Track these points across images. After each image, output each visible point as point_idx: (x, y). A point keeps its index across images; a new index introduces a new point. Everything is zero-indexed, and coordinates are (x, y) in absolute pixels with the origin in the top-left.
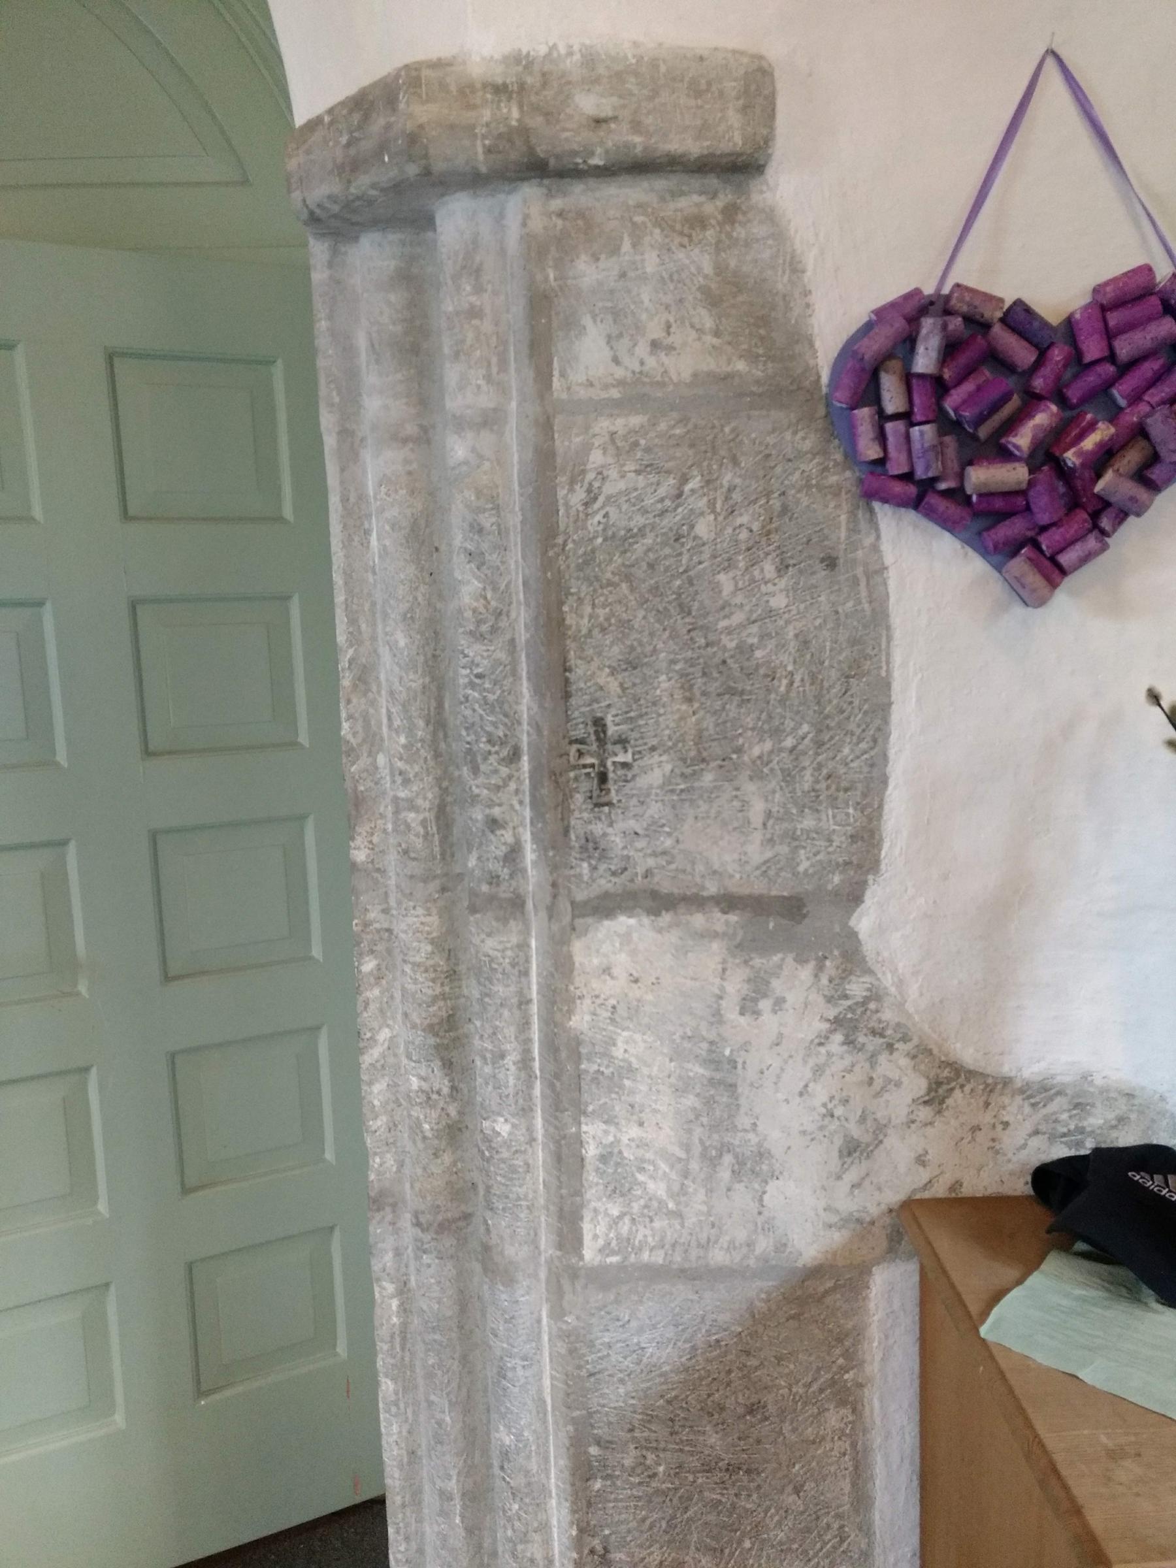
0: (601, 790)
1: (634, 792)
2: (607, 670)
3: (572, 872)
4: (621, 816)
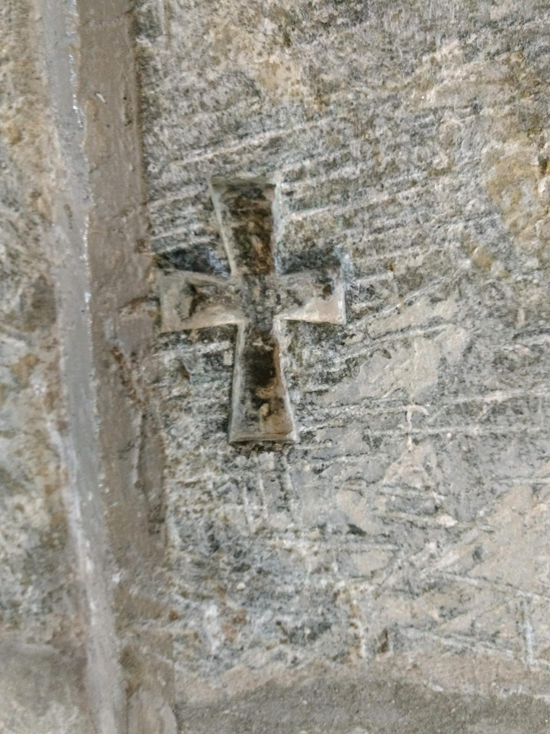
0: (258, 402)
1: (350, 410)
2: (269, 25)
3: (176, 629)
4: (312, 481)
